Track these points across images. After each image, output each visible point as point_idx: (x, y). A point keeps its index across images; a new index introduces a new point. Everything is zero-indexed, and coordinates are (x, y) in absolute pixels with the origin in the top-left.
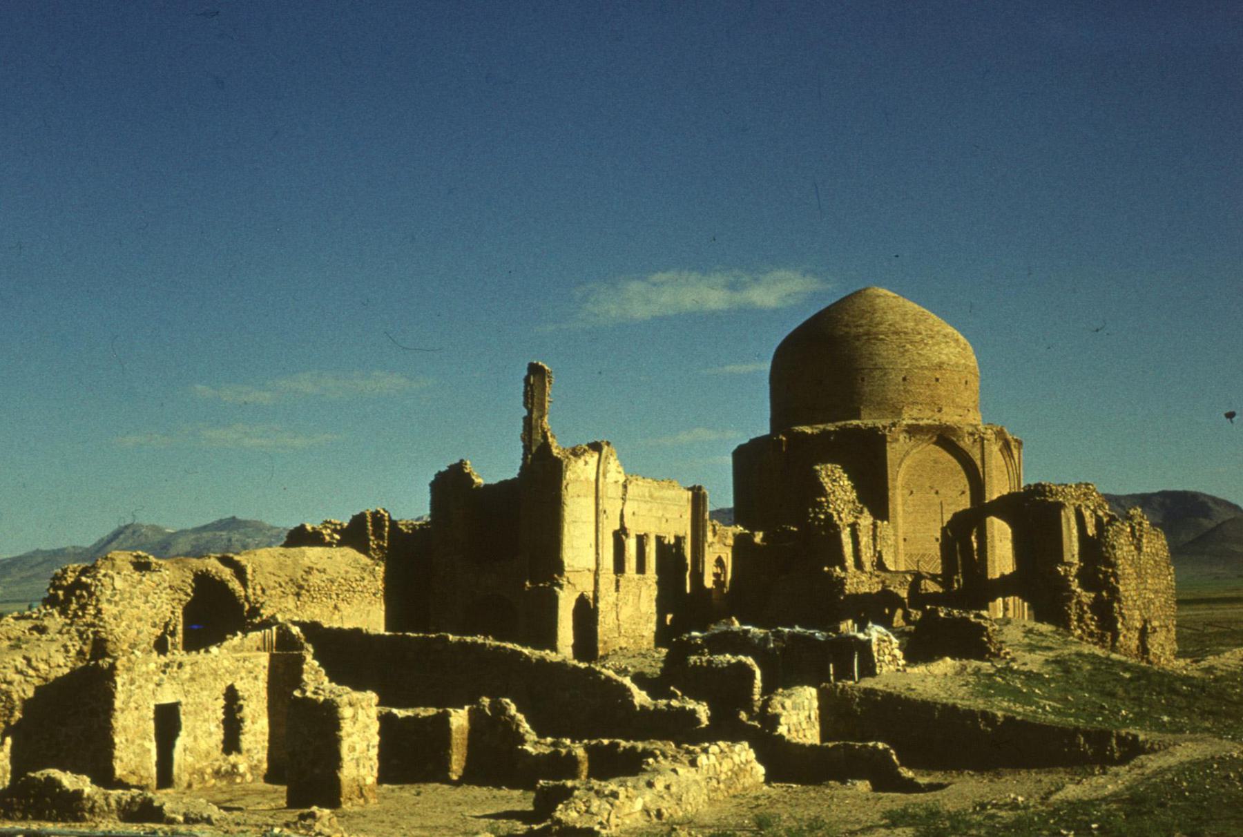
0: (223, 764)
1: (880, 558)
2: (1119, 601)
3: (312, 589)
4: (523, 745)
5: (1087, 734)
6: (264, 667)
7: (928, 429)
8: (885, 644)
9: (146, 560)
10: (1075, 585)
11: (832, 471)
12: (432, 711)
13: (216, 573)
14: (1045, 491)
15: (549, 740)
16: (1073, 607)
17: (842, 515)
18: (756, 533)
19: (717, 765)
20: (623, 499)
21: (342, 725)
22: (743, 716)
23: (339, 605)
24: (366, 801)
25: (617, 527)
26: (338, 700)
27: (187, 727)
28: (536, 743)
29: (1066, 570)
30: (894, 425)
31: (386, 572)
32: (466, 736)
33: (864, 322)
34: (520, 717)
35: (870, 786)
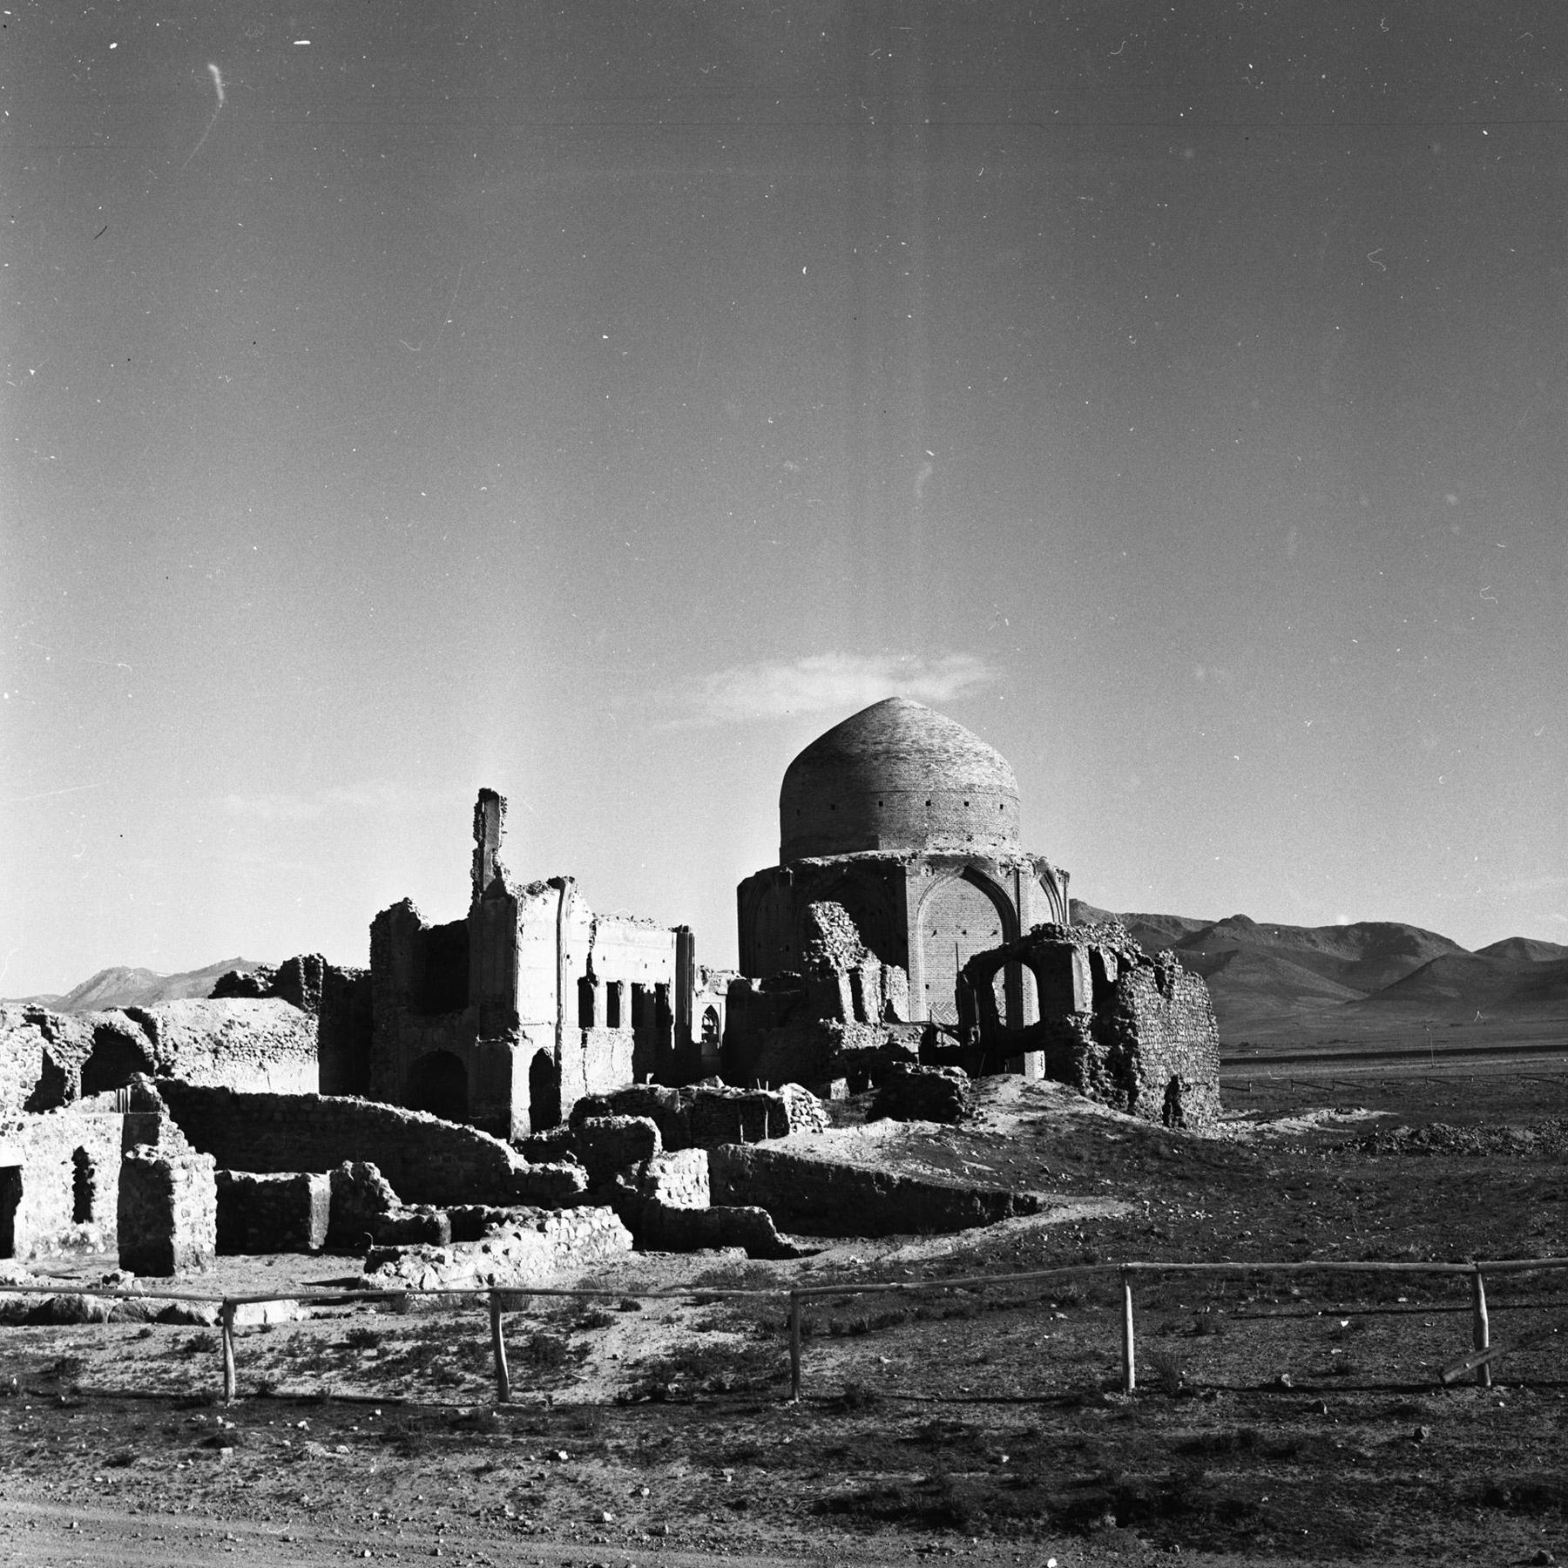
0: (70, 1233)
1: (890, 1006)
2: (1138, 1055)
3: (233, 1045)
4: (384, 1211)
5: (984, 1197)
6: (118, 1129)
7: (955, 860)
8: (803, 1103)
9: (41, 1013)
10: (1087, 1038)
11: (831, 909)
12: (292, 1176)
13: (122, 1027)
14: (1055, 932)
15: (414, 1206)
16: (1085, 1062)
17: (840, 960)
18: (754, 980)
19: (572, 1231)
20: (590, 941)
21: (174, 1187)
22: (620, 1180)
23: (264, 1063)
24: (203, 1269)
25: (584, 974)
26: (170, 1161)
27: (29, 1192)
28: (400, 1209)
29: (1076, 1020)
30: (914, 856)
31: (320, 1026)
32: (327, 1202)
33: (883, 738)
34: (384, 1182)
35: (745, 1253)
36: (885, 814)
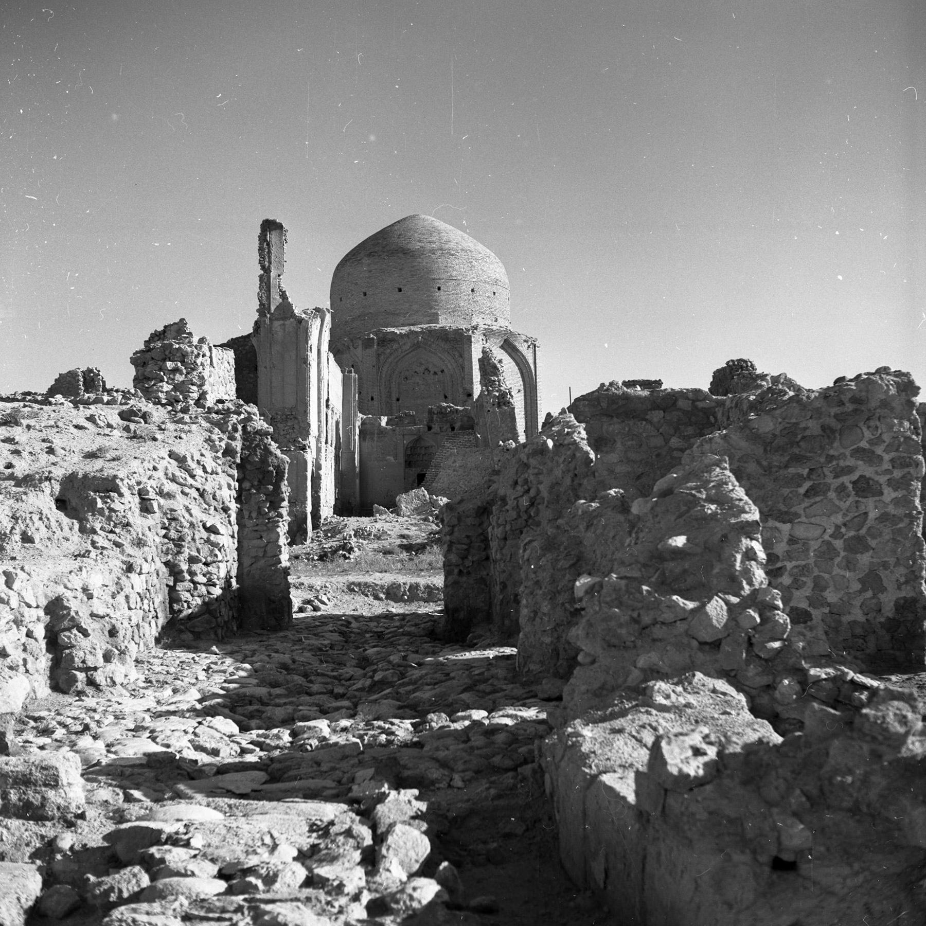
36: (442, 296)
